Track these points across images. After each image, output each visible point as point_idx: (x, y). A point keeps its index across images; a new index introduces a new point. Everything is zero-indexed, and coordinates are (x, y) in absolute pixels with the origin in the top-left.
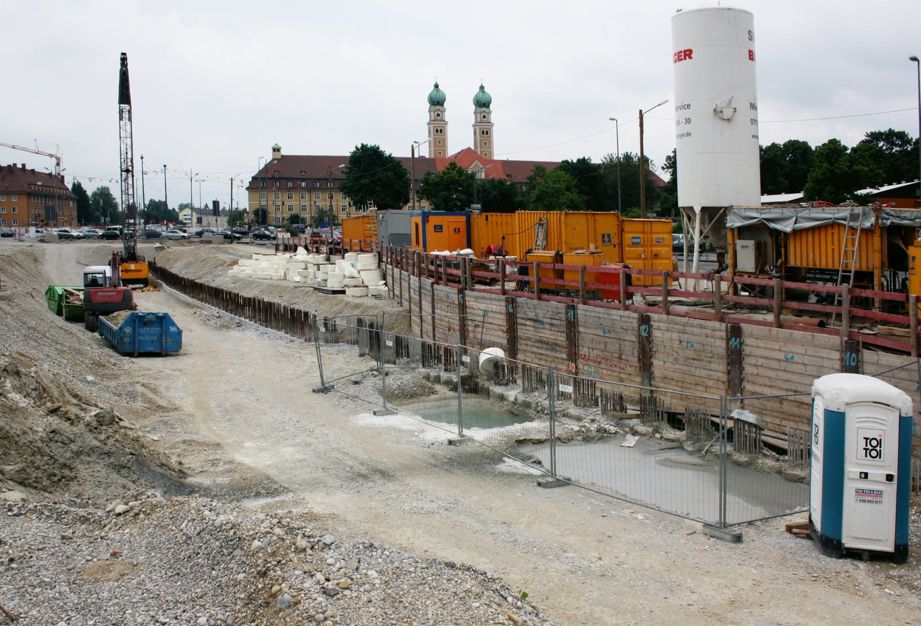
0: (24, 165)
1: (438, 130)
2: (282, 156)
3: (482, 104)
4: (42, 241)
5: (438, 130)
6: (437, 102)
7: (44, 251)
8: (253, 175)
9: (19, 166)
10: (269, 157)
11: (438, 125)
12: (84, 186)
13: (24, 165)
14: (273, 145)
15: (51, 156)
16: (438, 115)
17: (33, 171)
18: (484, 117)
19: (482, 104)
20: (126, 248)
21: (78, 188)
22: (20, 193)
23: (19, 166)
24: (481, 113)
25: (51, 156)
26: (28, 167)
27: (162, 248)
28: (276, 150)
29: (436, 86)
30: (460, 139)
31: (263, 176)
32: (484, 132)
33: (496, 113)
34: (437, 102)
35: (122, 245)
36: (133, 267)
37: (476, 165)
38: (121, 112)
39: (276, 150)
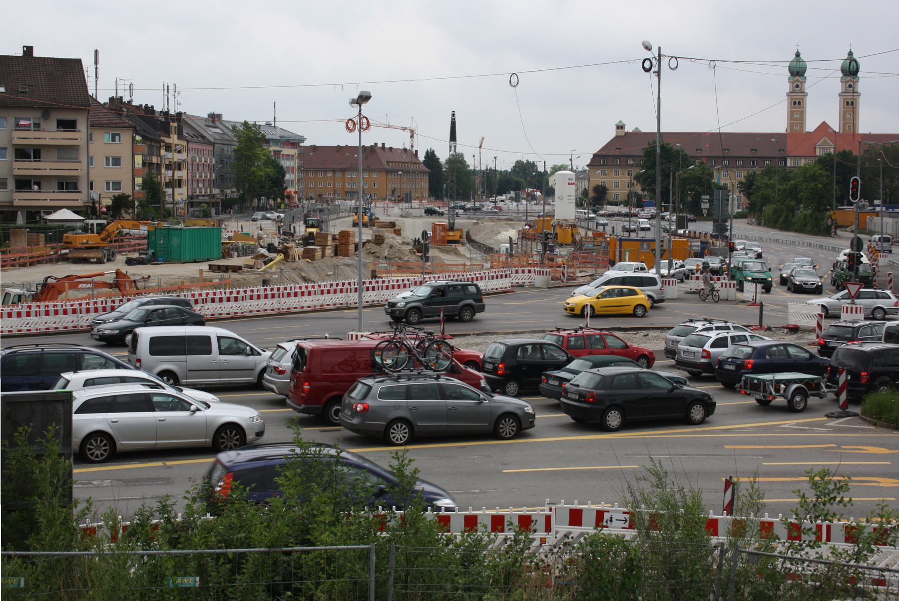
0: (383, 144)
1: (797, 103)
2: (627, 133)
3: (851, 70)
4: (402, 216)
5: (797, 103)
6: (797, 72)
7: (404, 223)
8: (596, 151)
9: (380, 145)
10: (611, 134)
11: (797, 97)
12: (438, 154)
13: (383, 144)
14: (617, 122)
15: (404, 129)
16: (797, 86)
17: (391, 149)
18: (797, 86)
19: (851, 70)
20: (450, 223)
21: (431, 156)
22: (379, 171)
23: (380, 145)
24: (846, 82)
25: (404, 129)
26: (387, 146)
27: (477, 223)
28: (620, 127)
29: (798, 55)
30: (822, 111)
31: (604, 153)
32: (850, 104)
33: (864, 83)
34: (797, 72)
35: (447, 221)
36: (451, 234)
37: (825, 141)
38: (450, 147)
39: (620, 127)
